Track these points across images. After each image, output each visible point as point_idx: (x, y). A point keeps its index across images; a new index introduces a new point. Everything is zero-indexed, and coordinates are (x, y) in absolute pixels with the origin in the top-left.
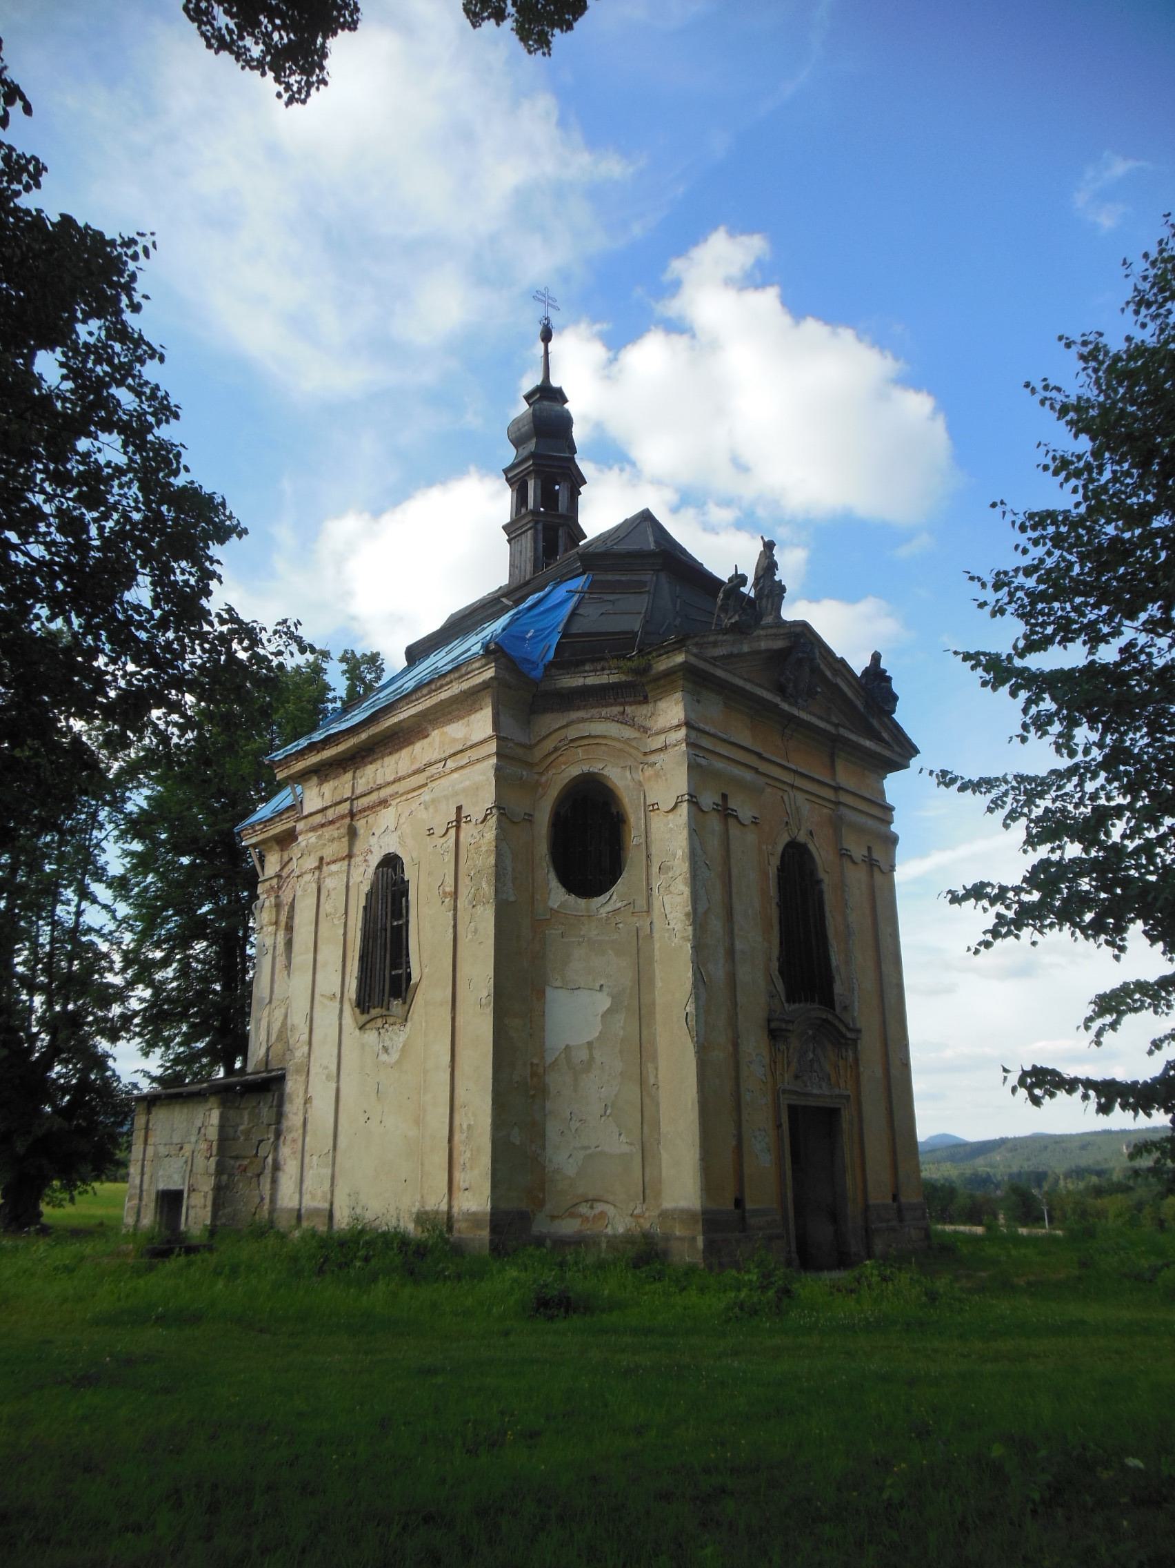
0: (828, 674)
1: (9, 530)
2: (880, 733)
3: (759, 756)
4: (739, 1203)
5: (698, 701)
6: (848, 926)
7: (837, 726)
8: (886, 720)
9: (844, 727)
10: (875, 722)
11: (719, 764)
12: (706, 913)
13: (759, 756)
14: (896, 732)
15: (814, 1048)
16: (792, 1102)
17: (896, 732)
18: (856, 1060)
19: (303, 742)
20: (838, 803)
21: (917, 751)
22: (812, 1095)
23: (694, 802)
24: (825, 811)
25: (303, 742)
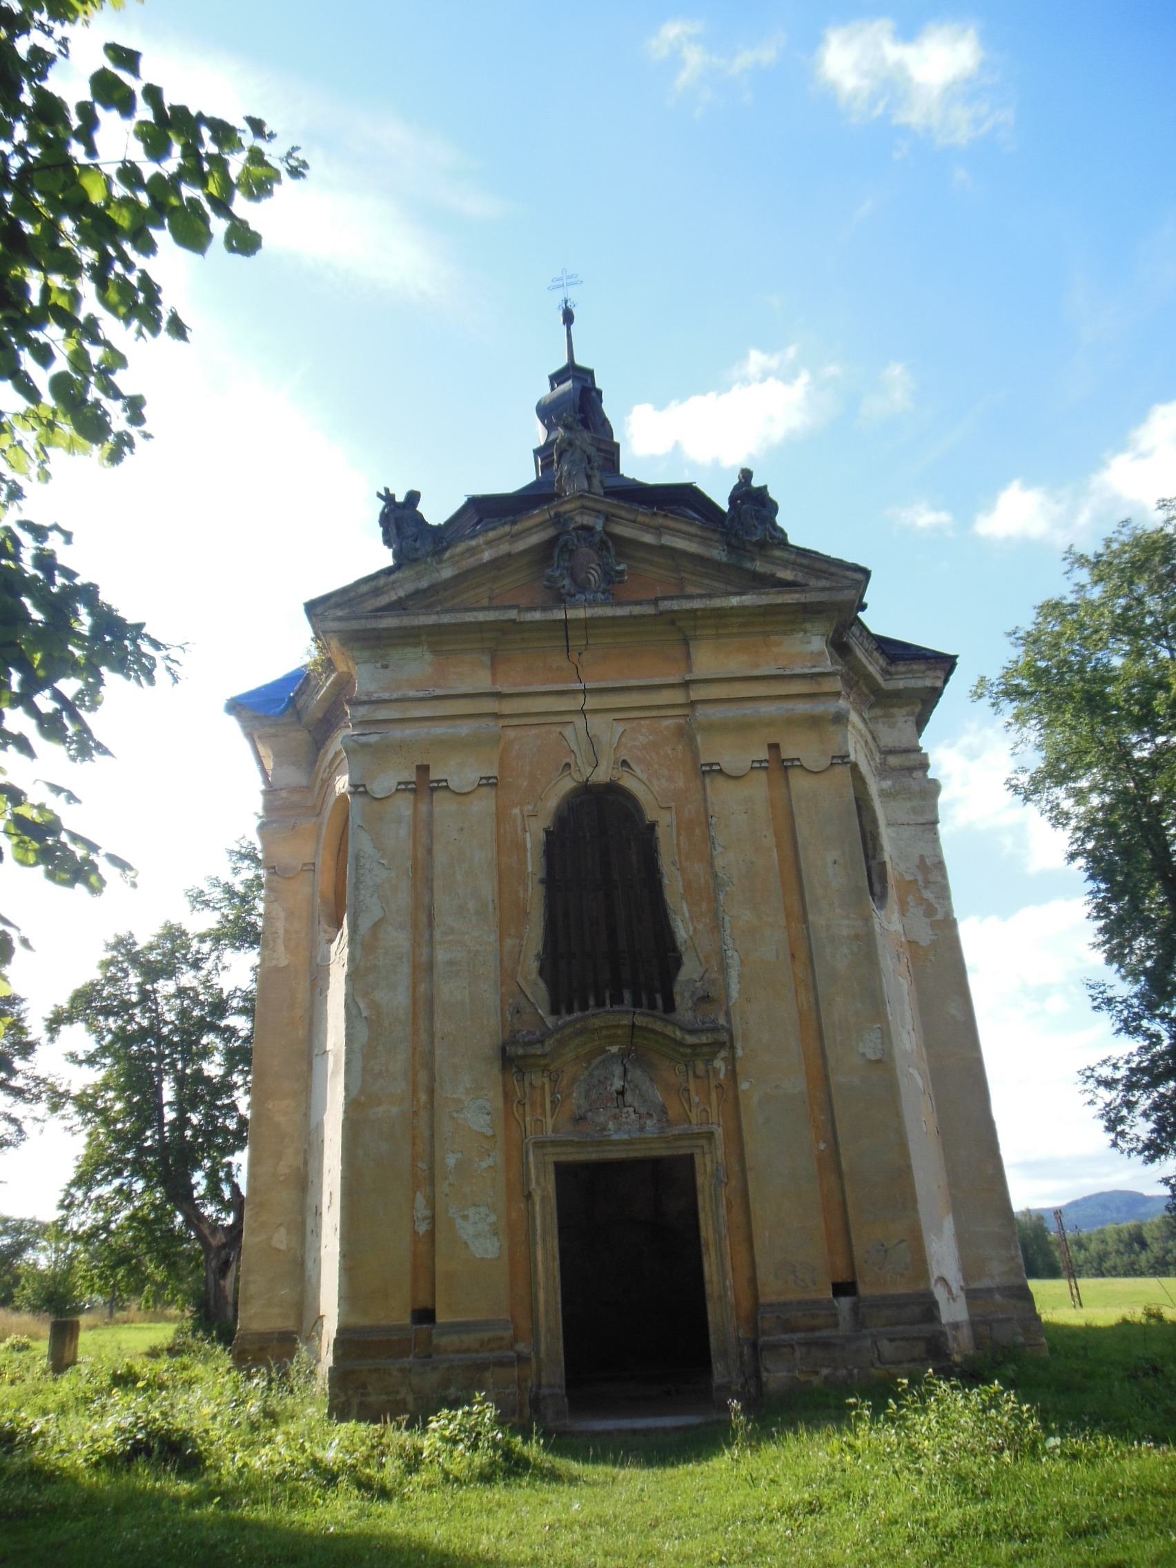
0: (648, 538)
1: (27, 596)
2: (773, 575)
3: (498, 695)
4: (425, 1315)
5: (385, 667)
6: (715, 876)
7: (655, 601)
8: (777, 553)
9: (665, 598)
10: (760, 566)
11: (398, 733)
12: (377, 926)
13: (498, 695)
14: (805, 561)
15: (625, 1071)
16: (563, 1158)
17: (805, 561)
18: (733, 1075)
19: (724, 1231)
20: (693, 704)
21: (866, 573)
22: (613, 1143)
23: (361, 793)
24: (670, 722)
25: (724, 1231)
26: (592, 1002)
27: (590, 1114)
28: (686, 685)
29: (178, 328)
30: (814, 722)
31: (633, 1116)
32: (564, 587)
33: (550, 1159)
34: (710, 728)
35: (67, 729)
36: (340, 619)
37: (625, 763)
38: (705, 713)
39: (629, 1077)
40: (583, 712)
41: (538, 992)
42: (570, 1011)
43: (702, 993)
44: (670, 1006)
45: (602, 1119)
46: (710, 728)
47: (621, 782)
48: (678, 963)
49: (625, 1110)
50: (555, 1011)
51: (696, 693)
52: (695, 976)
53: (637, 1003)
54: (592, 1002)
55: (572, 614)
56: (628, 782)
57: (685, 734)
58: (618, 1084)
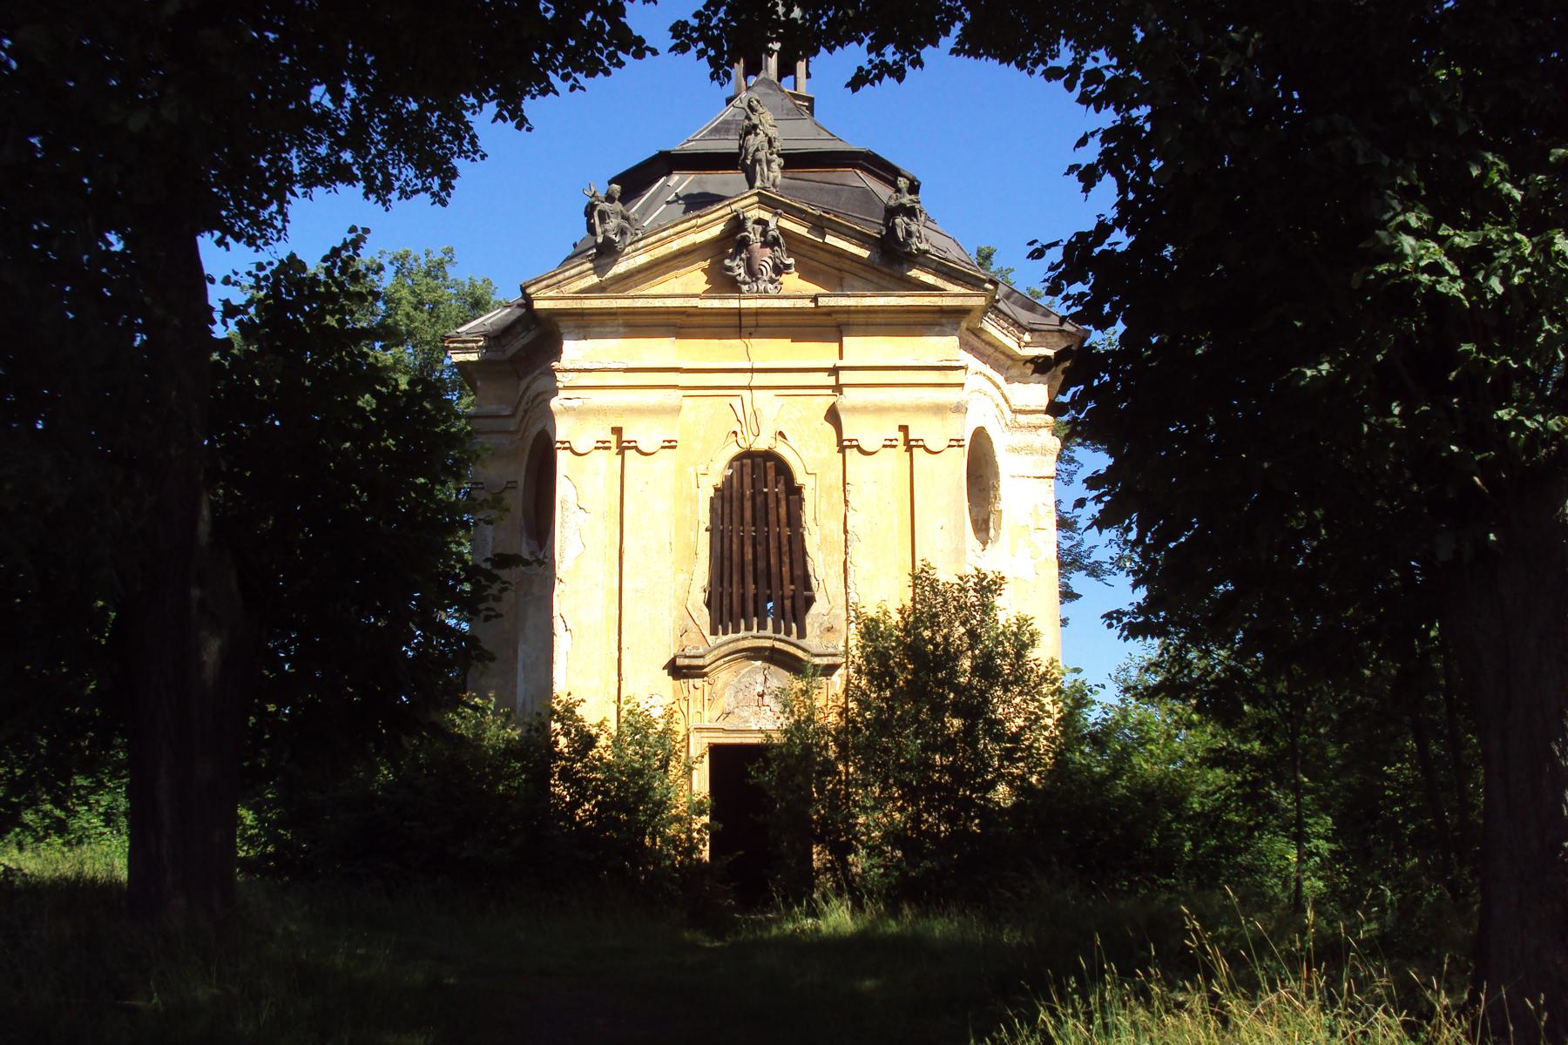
7: (819, 226)
26: (743, 626)
27: (736, 710)
28: (834, 371)
29: (387, 210)
30: (939, 410)
31: (769, 713)
32: (740, 275)
33: (706, 742)
34: (854, 410)
35: (331, 101)
36: (524, 704)
37: (781, 434)
38: (850, 397)
39: (768, 685)
40: (750, 388)
41: (704, 617)
42: (725, 633)
43: (827, 625)
44: (802, 634)
45: (746, 714)
46: (854, 410)
47: (775, 450)
48: (810, 601)
49: (763, 708)
50: (714, 632)
51: (845, 377)
52: (824, 612)
53: (776, 630)
54: (743, 626)
55: (745, 304)
56: (781, 449)
57: (833, 416)
58: (760, 689)
